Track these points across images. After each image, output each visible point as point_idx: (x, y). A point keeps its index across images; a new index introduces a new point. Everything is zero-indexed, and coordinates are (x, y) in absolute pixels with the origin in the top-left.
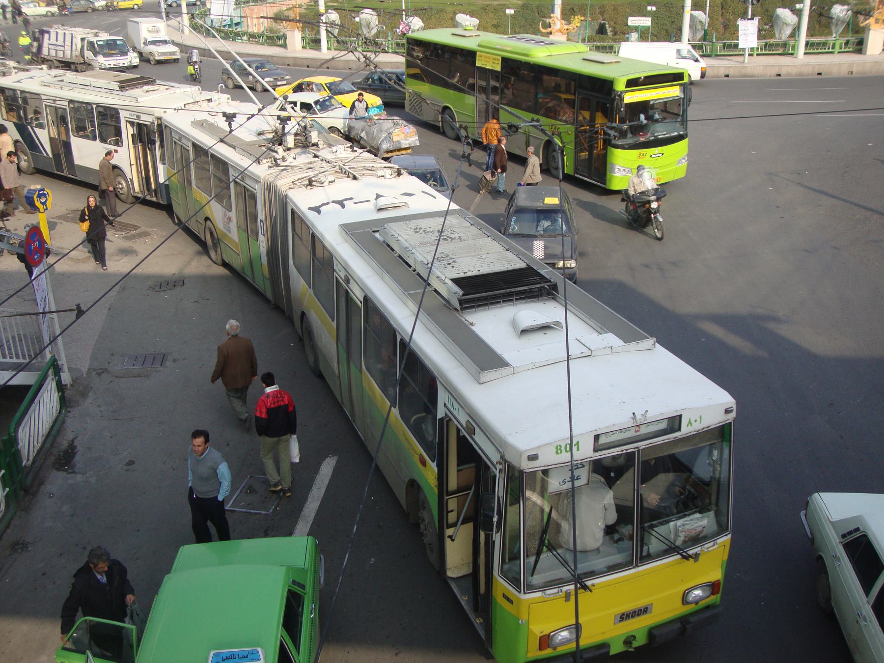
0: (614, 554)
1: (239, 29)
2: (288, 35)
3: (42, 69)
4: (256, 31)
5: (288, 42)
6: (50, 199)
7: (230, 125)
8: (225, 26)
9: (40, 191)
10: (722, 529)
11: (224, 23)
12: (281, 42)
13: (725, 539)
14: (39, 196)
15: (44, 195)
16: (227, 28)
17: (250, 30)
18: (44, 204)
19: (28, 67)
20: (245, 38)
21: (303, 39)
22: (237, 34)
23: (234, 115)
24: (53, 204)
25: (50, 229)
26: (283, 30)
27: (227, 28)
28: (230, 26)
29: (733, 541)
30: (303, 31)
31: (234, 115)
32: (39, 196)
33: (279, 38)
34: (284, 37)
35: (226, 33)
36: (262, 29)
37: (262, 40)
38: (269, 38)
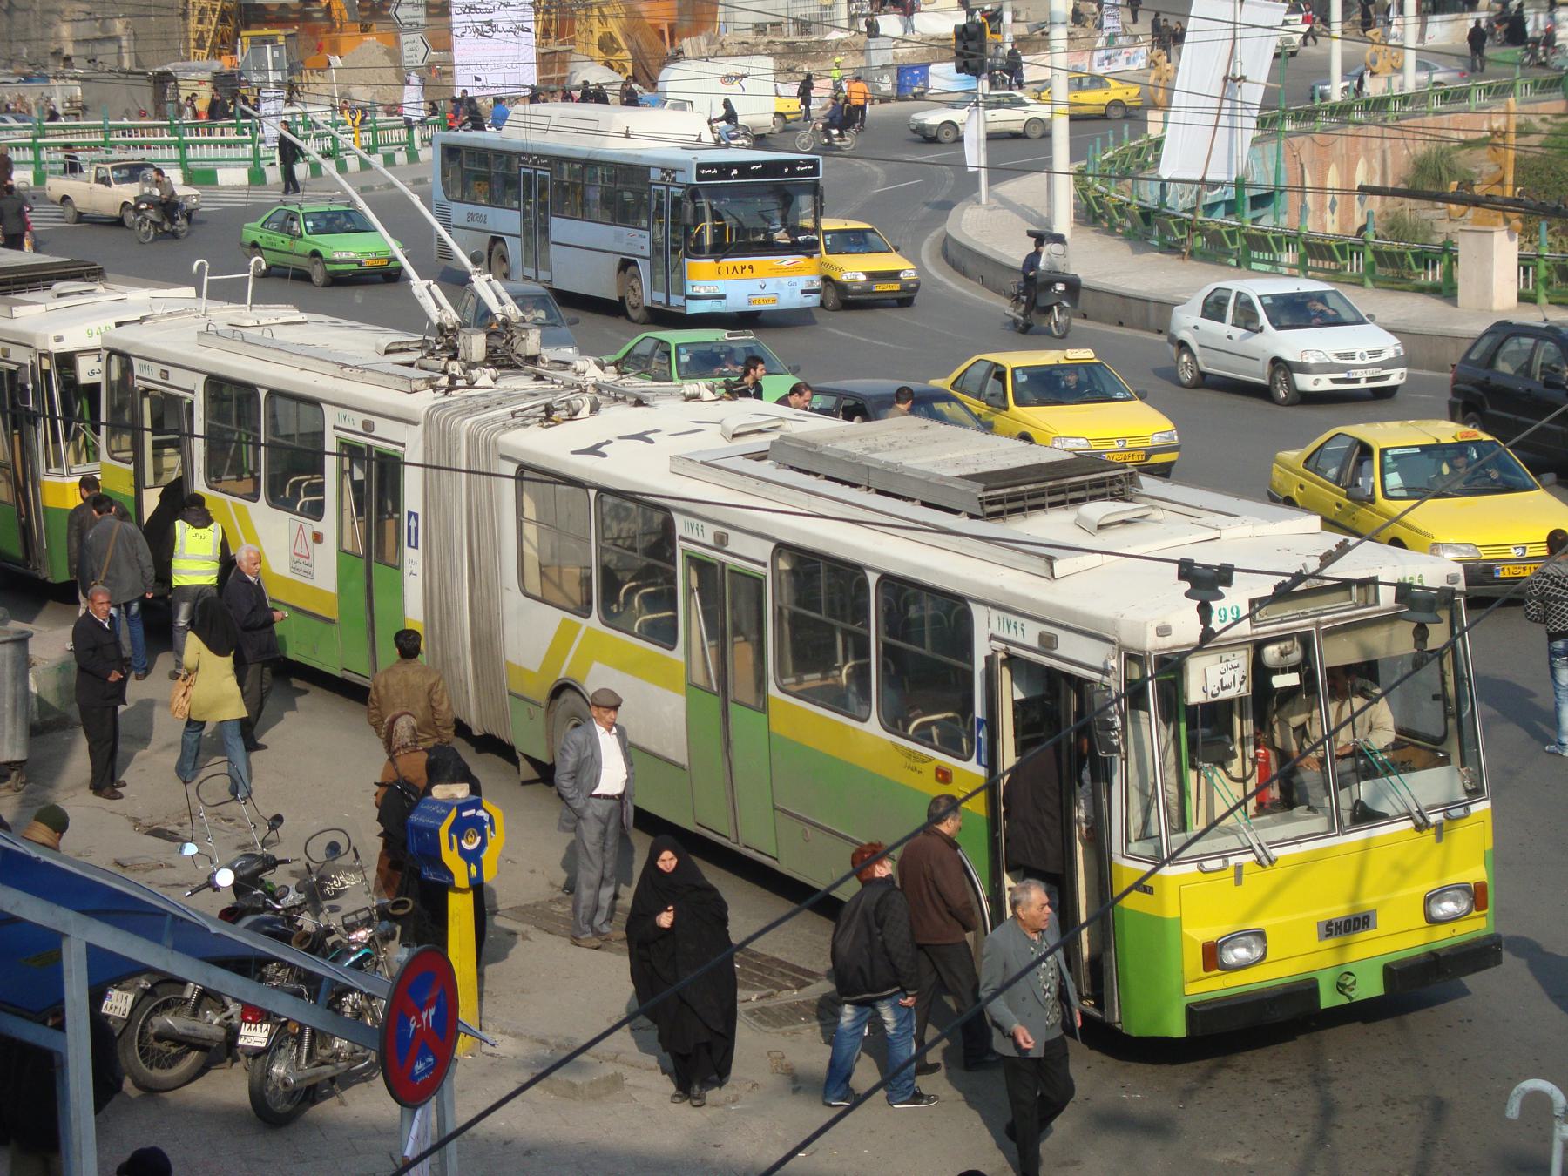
0: (1001, 292)
1: (1267, 222)
2: (1466, 247)
3: (695, 397)
4: (1332, 228)
5: (1463, 273)
6: (496, 841)
7: (1205, 612)
8: (1211, 208)
9: (463, 806)
10: (1475, 793)
11: (1211, 196)
12: (1434, 276)
13: (1482, 807)
14: (460, 828)
15: (477, 824)
16: (1219, 216)
17: (1310, 226)
18: (472, 857)
19: (635, 384)
20: (1288, 257)
21: (1525, 263)
22: (1258, 242)
23: (1224, 575)
24: (505, 860)
25: (481, 958)
26: (1446, 227)
27: (1219, 216)
28: (1231, 207)
29: (1495, 809)
30: (1528, 234)
31: (1224, 575)
32: (460, 828)
33: (1425, 259)
34: (1449, 252)
35: (1214, 238)
36: (1359, 221)
37: (1354, 266)
38: (1383, 258)
